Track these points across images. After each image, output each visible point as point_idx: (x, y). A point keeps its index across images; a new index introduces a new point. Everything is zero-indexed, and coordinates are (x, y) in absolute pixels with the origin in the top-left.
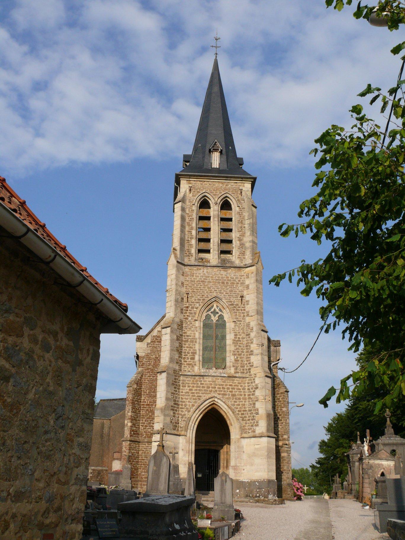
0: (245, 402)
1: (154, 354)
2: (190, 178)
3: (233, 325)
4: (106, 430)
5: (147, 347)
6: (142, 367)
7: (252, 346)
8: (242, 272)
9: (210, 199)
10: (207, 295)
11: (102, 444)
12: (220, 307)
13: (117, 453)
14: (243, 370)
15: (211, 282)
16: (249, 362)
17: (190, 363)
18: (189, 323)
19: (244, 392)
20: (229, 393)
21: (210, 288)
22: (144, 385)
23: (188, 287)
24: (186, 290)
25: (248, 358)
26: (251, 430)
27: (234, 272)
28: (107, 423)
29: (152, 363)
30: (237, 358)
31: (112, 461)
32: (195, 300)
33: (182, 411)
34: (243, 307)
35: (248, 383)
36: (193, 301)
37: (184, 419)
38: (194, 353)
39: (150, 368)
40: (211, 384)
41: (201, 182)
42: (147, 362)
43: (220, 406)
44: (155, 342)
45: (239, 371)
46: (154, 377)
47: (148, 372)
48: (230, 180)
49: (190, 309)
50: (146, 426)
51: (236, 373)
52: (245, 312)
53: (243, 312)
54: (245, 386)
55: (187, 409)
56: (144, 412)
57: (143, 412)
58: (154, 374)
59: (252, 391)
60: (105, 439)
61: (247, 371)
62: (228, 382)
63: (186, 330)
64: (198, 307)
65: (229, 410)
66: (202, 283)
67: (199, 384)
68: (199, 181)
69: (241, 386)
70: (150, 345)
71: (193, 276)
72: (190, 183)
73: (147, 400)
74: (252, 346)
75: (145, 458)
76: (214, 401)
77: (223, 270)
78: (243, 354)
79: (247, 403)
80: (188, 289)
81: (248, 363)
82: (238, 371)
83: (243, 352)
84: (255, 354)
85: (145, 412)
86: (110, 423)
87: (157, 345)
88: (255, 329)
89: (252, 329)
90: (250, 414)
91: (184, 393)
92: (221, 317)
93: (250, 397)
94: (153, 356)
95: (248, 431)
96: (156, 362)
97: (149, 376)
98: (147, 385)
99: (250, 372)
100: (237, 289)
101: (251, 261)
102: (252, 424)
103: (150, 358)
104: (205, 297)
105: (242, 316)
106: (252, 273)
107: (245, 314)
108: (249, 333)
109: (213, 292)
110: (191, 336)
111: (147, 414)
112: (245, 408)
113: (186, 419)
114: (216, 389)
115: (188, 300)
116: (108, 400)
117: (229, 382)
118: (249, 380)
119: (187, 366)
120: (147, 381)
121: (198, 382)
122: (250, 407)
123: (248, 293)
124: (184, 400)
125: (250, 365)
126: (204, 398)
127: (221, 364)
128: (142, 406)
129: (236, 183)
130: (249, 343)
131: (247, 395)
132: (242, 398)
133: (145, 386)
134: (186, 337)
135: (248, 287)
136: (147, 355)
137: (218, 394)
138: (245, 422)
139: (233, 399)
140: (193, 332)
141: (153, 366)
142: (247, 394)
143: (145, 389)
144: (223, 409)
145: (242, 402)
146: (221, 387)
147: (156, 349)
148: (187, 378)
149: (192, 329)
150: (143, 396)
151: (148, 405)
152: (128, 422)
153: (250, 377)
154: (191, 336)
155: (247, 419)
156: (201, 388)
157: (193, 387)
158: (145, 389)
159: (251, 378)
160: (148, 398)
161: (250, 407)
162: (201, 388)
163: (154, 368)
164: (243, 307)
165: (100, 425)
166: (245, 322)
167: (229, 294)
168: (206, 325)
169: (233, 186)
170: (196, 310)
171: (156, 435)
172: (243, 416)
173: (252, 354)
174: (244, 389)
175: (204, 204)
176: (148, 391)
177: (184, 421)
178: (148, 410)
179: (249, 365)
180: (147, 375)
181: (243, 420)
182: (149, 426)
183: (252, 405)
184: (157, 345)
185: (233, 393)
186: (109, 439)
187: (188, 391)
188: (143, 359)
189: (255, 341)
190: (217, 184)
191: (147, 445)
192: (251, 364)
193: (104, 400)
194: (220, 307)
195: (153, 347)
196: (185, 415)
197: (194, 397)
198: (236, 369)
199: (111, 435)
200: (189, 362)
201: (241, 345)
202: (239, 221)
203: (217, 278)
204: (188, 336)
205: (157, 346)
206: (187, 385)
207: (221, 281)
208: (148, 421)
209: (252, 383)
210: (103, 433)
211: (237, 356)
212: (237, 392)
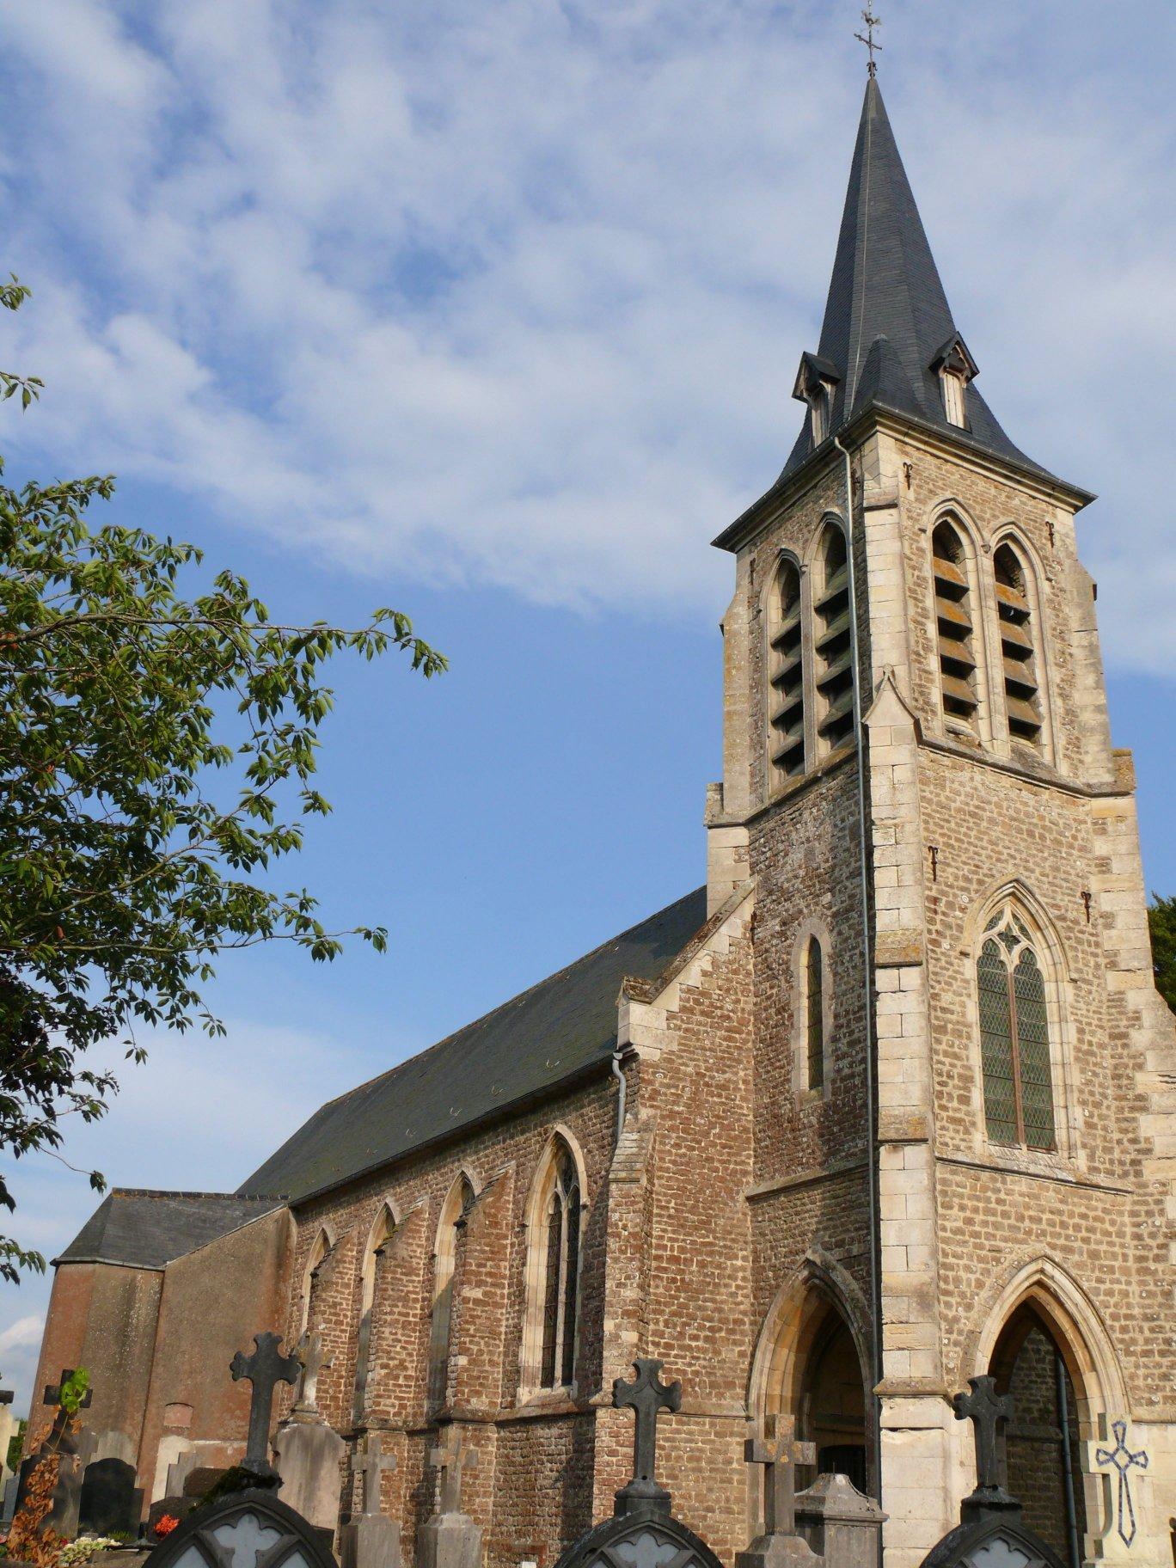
0: (1128, 1283)
1: (691, 1060)
2: (906, 434)
3: (1069, 991)
4: (142, 1312)
5: (669, 1028)
6: (652, 1106)
7: (1139, 1077)
8: (1081, 808)
9: (965, 529)
10: (990, 869)
11: (120, 1366)
12: (1025, 919)
13: (178, 1408)
14: (1112, 1162)
15: (997, 824)
16: (1131, 1136)
17: (958, 1115)
18: (943, 963)
19: (1123, 1246)
20: (1079, 1244)
21: (997, 845)
22: (660, 1178)
23: (931, 827)
24: (926, 834)
25: (1126, 1120)
26: (1159, 1394)
27: (1058, 802)
28: (146, 1283)
29: (687, 1095)
30: (1092, 1116)
31: (157, 1438)
32: (956, 878)
33: (948, 1305)
34: (1092, 935)
35: (1134, 1214)
36: (951, 879)
37: (954, 1337)
38: (967, 1080)
39: (678, 1113)
40: (1027, 1207)
41: (938, 462)
42: (668, 1086)
43: (1060, 1293)
44: (693, 1013)
45: (1101, 1167)
46: (693, 1149)
47: (672, 1129)
48: (1019, 482)
49: (944, 909)
50: (669, 1346)
51: (1093, 1170)
52: (1099, 951)
53: (1093, 949)
54: (1123, 1224)
55: (963, 1295)
56: (661, 1290)
57: (657, 1287)
58: (693, 1140)
59: (1153, 1243)
60: (138, 1347)
61: (1127, 1167)
62: (1074, 1204)
63: (938, 986)
64: (966, 908)
65: (1089, 1313)
66: (971, 820)
67: (993, 1200)
68: (933, 455)
69: (1113, 1223)
70: (679, 1023)
71: (943, 787)
72: (906, 454)
73: (670, 1239)
74: (1139, 1077)
75: (667, 1477)
76: (1042, 1271)
77: (1028, 790)
78: (1105, 1103)
79: (1134, 1288)
80: (934, 832)
81: (1125, 1138)
82: (1097, 1164)
83: (1106, 1097)
84: (1155, 1108)
85: (665, 1287)
86: (162, 1284)
87: (700, 1024)
88: (1147, 1018)
89: (1138, 1019)
90: (1152, 1330)
91: (948, 1234)
92: (1028, 958)
93: (1144, 1264)
94: (687, 1066)
95: (1146, 1395)
96: (697, 1089)
97: (677, 1146)
98: (669, 1179)
99: (1138, 1174)
100: (1072, 867)
101: (1108, 778)
102: (1164, 1370)
103: (678, 1071)
104: (985, 875)
105: (1092, 964)
106: (1120, 818)
107: (1102, 961)
108: (1123, 1030)
109: (1006, 861)
110: (952, 1013)
111: (671, 1297)
112: (1129, 1306)
113: (962, 1338)
114: (1044, 1226)
115: (935, 874)
116: (143, 1193)
117: (1078, 1204)
118: (1135, 1203)
119: (951, 1127)
120: (670, 1161)
121: (989, 1194)
122: (1150, 1307)
123: (1107, 887)
124: (951, 1260)
125: (1137, 1147)
126: (1008, 1259)
127: (1041, 1135)
128: (654, 1264)
129: (1034, 498)
130: (1126, 1066)
131: (1131, 1259)
132: (1120, 1268)
133: (663, 1182)
134: (939, 1014)
135: (1104, 865)
136: (670, 1061)
137: (1049, 1244)
138: (1133, 1359)
139: (1093, 1271)
140: (958, 999)
141: (688, 1106)
142: (1131, 1253)
143: (665, 1195)
144: (1069, 1305)
145: (1118, 1282)
146: (1057, 1218)
147: (698, 1040)
148: (954, 1173)
149: (955, 987)
150: (657, 1222)
151: (674, 1260)
152: (618, 1327)
153: (1141, 1191)
154: (952, 1013)
155: (1139, 1349)
156: (999, 1219)
157: (976, 1210)
158: (665, 1195)
159: (1146, 1195)
160: (674, 1232)
161: (1150, 1307)
162: (999, 1219)
163: (691, 1114)
164: (1092, 935)
165: (120, 1291)
166: (1105, 989)
167: (1051, 879)
168: (989, 984)
169: (1025, 504)
170: (960, 915)
171: (898, 1400)
172: (1126, 1337)
173: (1144, 1109)
174: (1121, 1234)
175: (945, 542)
176: (672, 1205)
177: (956, 1344)
178: (674, 1280)
179: (1131, 1147)
180: (669, 1137)
181: (1128, 1353)
182: (681, 1347)
183: (1160, 1299)
184: (700, 1024)
185: (1093, 1246)
186: (153, 1350)
187: (960, 1224)
188: (654, 1073)
189: (1151, 1060)
190: (981, 485)
191: (674, 1426)
192: (1143, 1145)
193: (129, 1192)
194: (1025, 919)
195: (687, 1030)
196: (956, 1320)
197: (983, 1253)
198: (1091, 1157)
199: (162, 1333)
200: (956, 1110)
201: (1098, 1070)
202: (1055, 629)
203: (1012, 812)
204: (944, 1010)
205: (702, 1028)
206: (956, 1200)
207: (1024, 827)
208: (675, 1326)
209: (1149, 1214)
210: (127, 1325)
211: (1090, 1108)
212: (1101, 1243)
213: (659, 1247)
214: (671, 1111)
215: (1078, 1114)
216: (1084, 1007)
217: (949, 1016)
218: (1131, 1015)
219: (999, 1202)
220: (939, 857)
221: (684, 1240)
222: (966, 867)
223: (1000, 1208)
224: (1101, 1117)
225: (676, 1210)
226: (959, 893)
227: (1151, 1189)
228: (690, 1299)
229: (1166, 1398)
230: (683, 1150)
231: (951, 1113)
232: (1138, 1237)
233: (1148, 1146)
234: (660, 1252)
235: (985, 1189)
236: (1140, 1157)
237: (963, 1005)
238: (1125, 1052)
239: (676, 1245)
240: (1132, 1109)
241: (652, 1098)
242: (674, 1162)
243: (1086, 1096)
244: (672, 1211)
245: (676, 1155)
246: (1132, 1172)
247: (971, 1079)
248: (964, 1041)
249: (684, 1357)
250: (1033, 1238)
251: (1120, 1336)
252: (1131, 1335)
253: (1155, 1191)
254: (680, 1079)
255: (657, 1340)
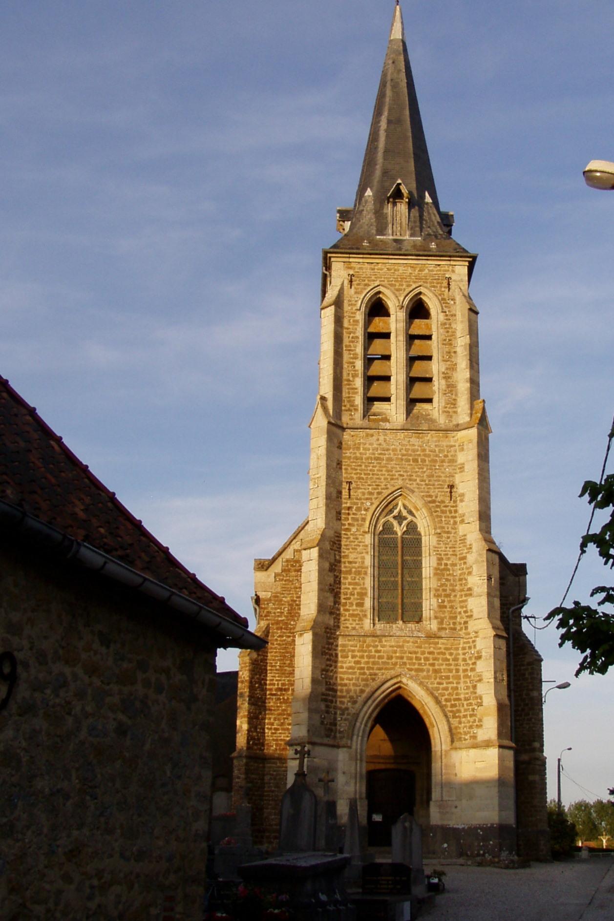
6: (267, 620)
10: (386, 485)
16: (465, 609)
18: (352, 539)
30: (443, 601)
32: (364, 494)
36: (360, 495)
38: (362, 595)
46: (289, 637)
51: (440, 629)
53: (453, 514)
67: (373, 651)
69: (451, 654)
73: (277, 680)
75: (275, 788)
82: (444, 626)
85: (275, 703)
88: (474, 549)
89: (471, 548)
99: (466, 628)
103: (281, 600)
120: (277, 644)
122: (467, 693)
136: (276, 597)
147: (292, 584)
148: (349, 640)
149: (358, 550)
153: (467, 637)
154: (356, 563)
158: (273, 660)
160: (278, 677)
172: (454, 709)
173: (471, 595)
177: (346, 720)
182: (283, 729)
183: (471, 690)
188: (268, 604)
192: (469, 614)
195: (285, 581)
196: (347, 709)
200: (354, 610)
201: (449, 577)
203: (404, 452)
204: (350, 562)
207: (411, 458)
212: (442, 665)
213: (270, 684)
214: (278, 620)
215: (434, 601)
216: (444, 546)
217: (354, 565)
218: (468, 546)
219: (377, 651)
220: (353, 485)
221: (284, 680)
222: (370, 487)
223: (377, 655)
224: (450, 601)
225: (280, 666)
226: (365, 501)
227: (471, 635)
228: (287, 707)
229: (471, 737)
230: (284, 638)
231: (351, 612)
232: (465, 660)
233: (471, 614)
234: (271, 687)
235: (368, 646)
236: (468, 619)
237: (363, 558)
238: (465, 567)
239: (280, 682)
240: (466, 595)
241: (266, 616)
242: (279, 644)
243: (440, 592)
244: (278, 667)
245: (280, 641)
246: (464, 628)
247: (366, 594)
248: (363, 576)
249: (285, 733)
250: (398, 666)
251: (451, 709)
252: (458, 708)
253: (473, 636)
254: (283, 605)
255: (270, 727)
